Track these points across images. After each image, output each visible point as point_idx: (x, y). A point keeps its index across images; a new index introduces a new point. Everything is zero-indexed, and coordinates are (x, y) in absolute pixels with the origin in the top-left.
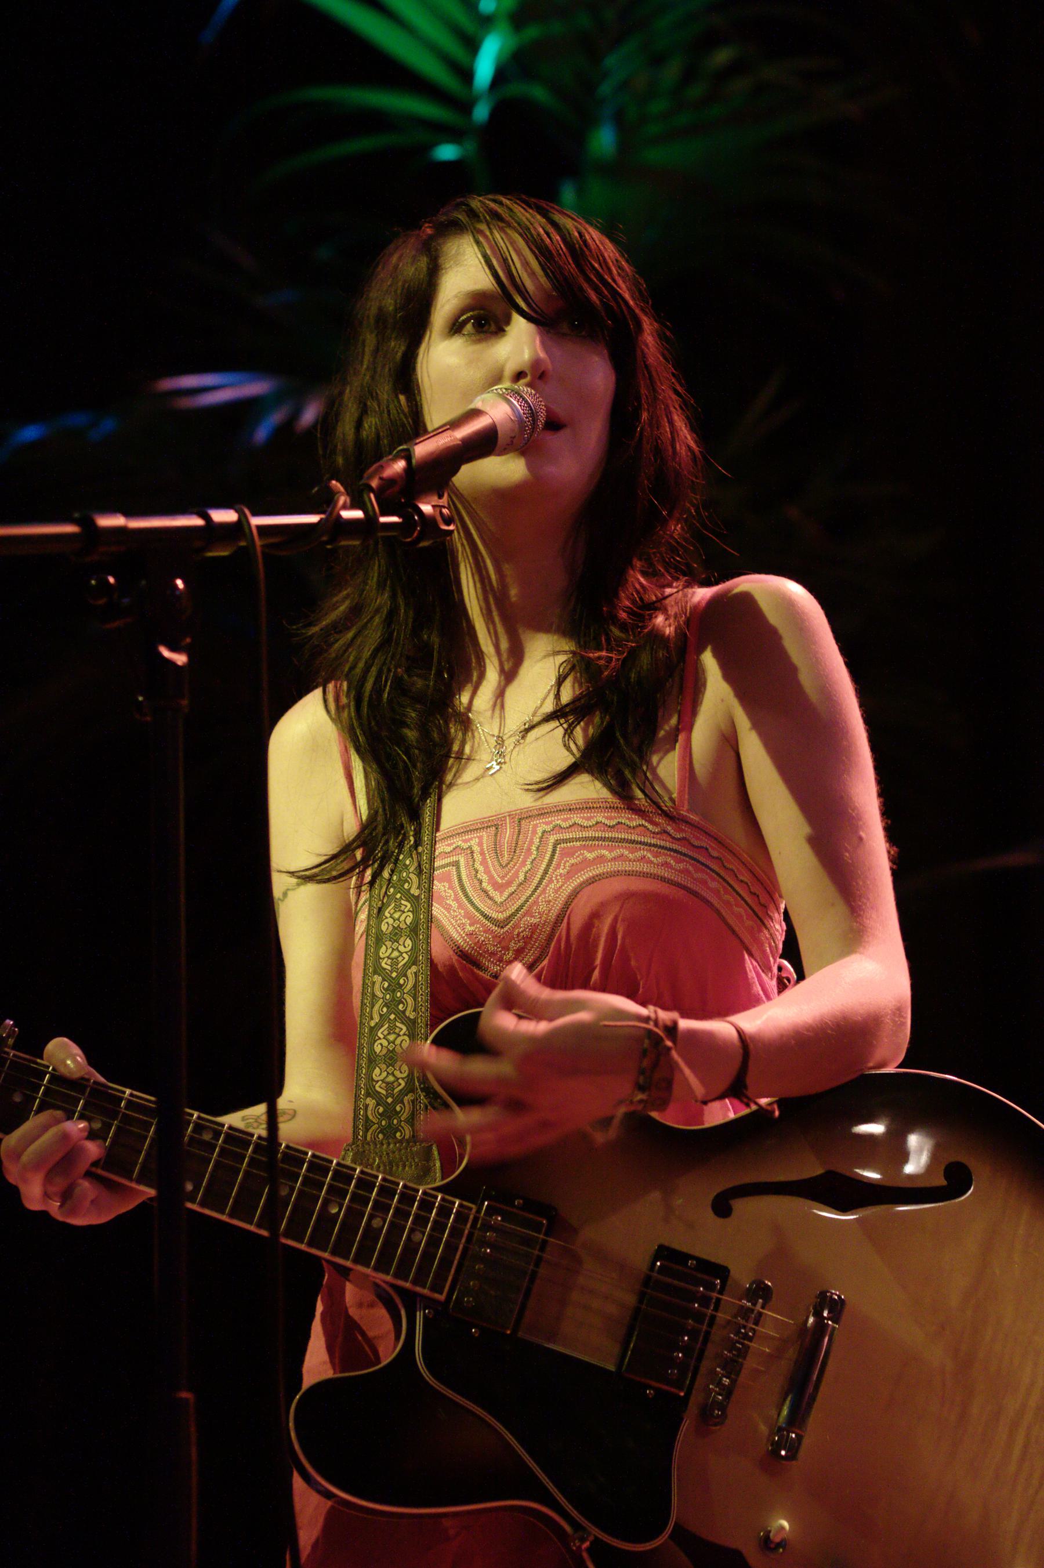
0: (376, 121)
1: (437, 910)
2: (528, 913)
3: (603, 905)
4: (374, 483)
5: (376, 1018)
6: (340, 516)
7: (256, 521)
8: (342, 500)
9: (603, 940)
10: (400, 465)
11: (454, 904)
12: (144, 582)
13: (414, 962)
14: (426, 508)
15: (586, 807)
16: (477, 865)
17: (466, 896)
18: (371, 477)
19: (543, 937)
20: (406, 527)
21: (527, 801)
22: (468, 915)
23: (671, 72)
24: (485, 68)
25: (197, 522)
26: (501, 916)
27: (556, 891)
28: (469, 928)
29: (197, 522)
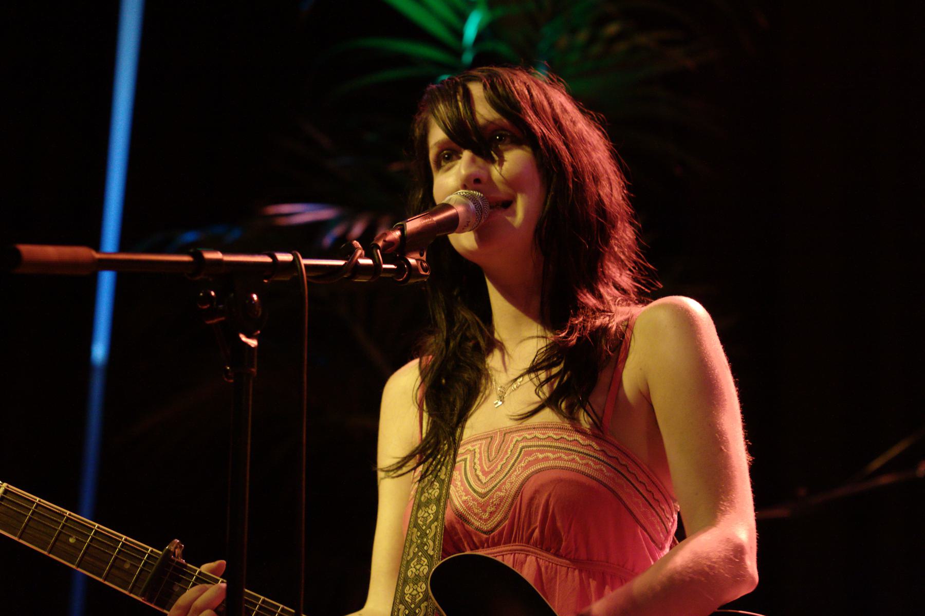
0: (404, 60)
1: (452, 489)
2: (500, 490)
3: (543, 486)
4: (380, 244)
5: (411, 555)
6: (357, 262)
7: (304, 262)
8: (360, 252)
9: (541, 507)
10: (397, 234)
11: (459, 484)
12: (232, 295)
13: (436, 519)
14: (412, 261)
15: (544, 427)
16: (476, 461)
17: (467, 479)
18: (379, 239)
19: (507, 505)
20: (399, 272)
21: (510, 424)
22: (465, 491)
23: (582, 37)
24: (471, 30)
25: (268, 259)
26: (483, 491)
27: (517, 476)
28: (464, 498)
29: (268, 259)
